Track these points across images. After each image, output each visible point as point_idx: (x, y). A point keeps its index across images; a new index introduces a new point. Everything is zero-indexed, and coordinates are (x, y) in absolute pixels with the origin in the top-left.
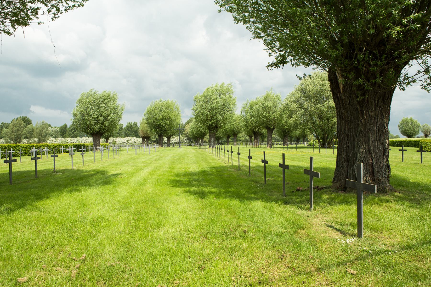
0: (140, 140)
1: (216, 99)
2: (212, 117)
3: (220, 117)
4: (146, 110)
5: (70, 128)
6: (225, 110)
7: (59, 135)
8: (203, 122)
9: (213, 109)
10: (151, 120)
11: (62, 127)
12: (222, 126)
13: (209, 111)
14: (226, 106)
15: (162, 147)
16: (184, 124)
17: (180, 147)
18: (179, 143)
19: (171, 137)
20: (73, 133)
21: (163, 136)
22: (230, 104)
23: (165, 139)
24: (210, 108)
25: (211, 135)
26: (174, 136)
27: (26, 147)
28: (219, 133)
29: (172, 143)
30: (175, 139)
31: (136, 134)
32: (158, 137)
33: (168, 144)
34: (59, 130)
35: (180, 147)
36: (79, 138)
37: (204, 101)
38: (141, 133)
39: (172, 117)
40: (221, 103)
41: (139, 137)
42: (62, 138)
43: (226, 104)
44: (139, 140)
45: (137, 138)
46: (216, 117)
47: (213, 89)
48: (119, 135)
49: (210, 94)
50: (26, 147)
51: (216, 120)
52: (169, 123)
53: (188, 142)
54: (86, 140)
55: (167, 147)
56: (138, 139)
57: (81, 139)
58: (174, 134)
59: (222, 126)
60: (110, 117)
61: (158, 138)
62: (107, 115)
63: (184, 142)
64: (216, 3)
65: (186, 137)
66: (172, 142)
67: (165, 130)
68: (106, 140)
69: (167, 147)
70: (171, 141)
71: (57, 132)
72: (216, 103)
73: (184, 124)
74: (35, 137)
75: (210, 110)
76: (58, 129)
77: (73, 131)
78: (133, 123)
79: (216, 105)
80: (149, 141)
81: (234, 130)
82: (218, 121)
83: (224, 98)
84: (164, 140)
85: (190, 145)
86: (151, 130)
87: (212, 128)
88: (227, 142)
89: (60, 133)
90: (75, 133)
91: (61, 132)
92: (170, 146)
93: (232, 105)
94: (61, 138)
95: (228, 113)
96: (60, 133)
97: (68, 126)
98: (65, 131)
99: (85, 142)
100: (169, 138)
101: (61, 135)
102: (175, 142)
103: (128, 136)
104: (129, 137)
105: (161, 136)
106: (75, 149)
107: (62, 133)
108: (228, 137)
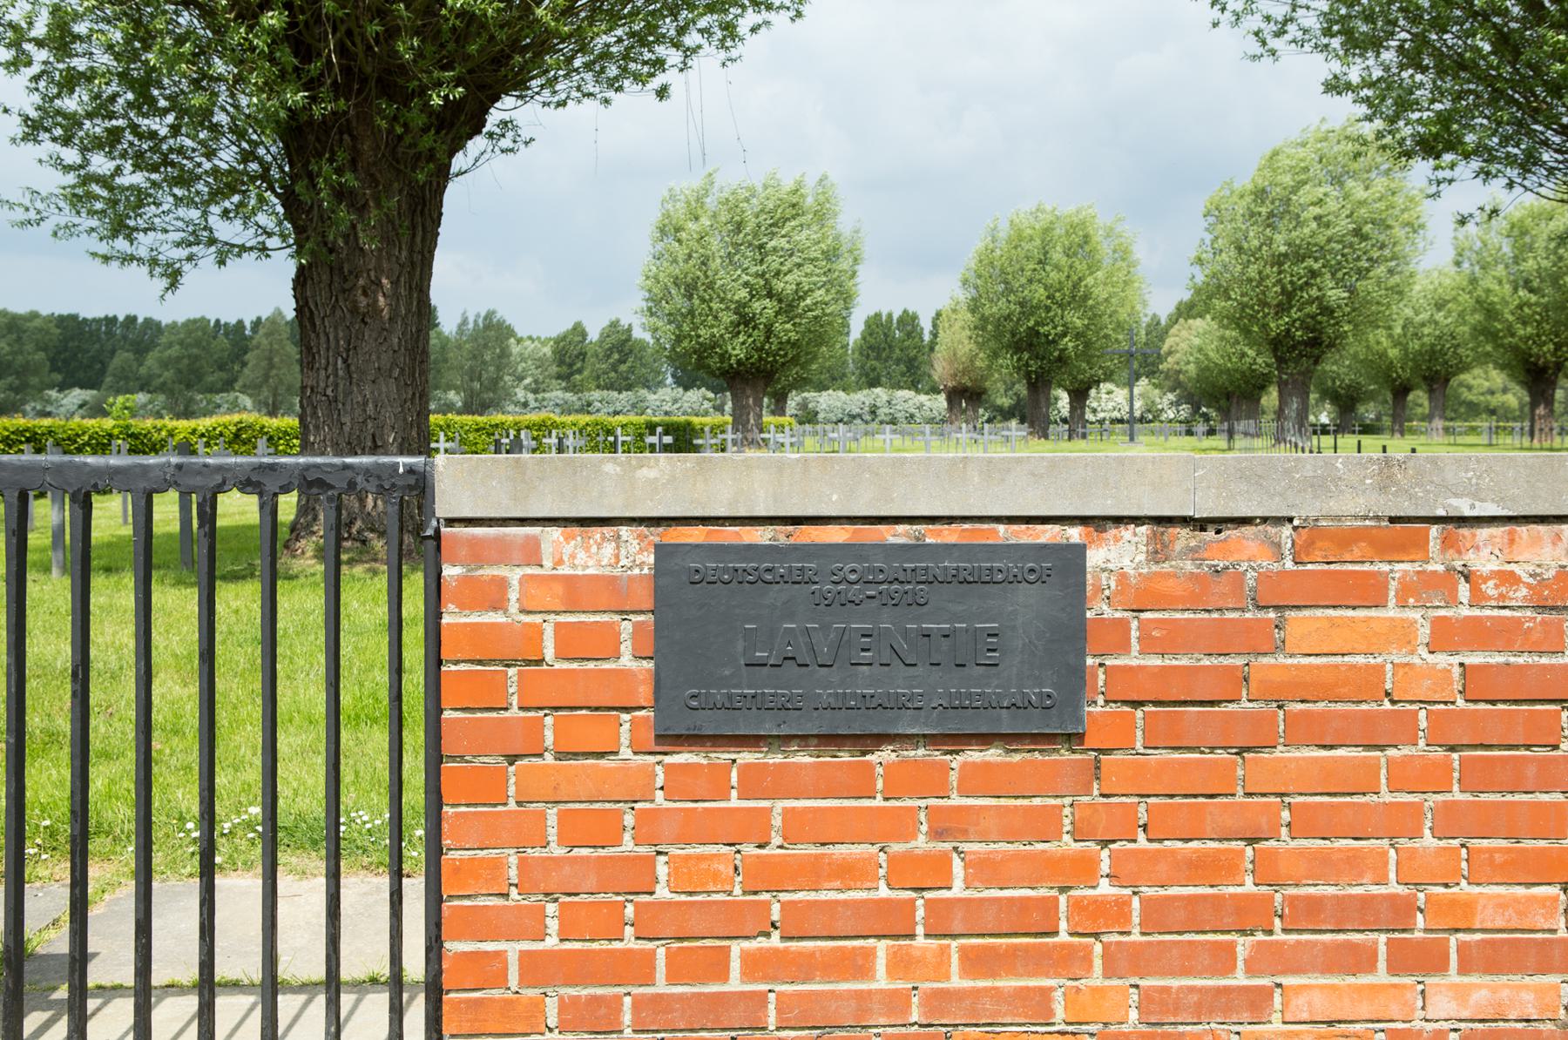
0: (941, 401)
1: (1319, 202)
2: (1289, 295)
3: (1335, 295)
4: (969, 260)
5: (601, 342)
6: (1358, 260)
7: (551, 377)
8: (1242, 320)
9: (1298, 254)
10: (999, 308)
11: (564, 338)
12: (1344, 335)
13: (1279, 260)
14: (1365, 238)
15: (1046, 437)
16: (1163, 322)
17: (1132, 439)
18: (1131, 424)
19: (1093, 392)
20: (614, 368)
21: (1048, 385)
22: (1389, 227)
23: (1063, 401)
24: (1283, 249)
25: (1286, 383)
26: (1105, 387)
27: (477, 430)
28: (1337, 367)
29: (1101, 422)
30: (1109, 399)
31: (913, 373)
32: (1022, 389)
33: (1076, 425)
34: (549, 354)
35: (1132, 439)
36: (643, 392)
37: (1252, 215)
38: (941, 369)
39: (1101, 293)
40: (1343, 226)
41: (934, 390)
42: (566, 389)
43: (1367, 228)
44: (928, 404)
45: (918, 391)
46: (1314, 292)
47: (1302, 152)
48: (833, 379)
49: (1287, 180)
50: (477, 430)
51: (1314, 308)
52: (1078, 323)
53: (1184, 415)
54: (675, 401)
55: (1070, 438)
56: (923, 398)
57: (651, 397)
58: (1109, 377)
59: (1344, 335)
60: (808, 301)
61: (1024, 392)
62: (796, 292)
63: (1164, 417)
64: (1213, 5)
65: (1172, 390)
66: (1101, 415)
67: (1060, 359)
68: (778, 401)
69: (1070, 438)
70: (1094, 411)
71: (540, 363)
72: (1314, 225)
73: (1163, 322)
74: (449, 387)
75: (1286, 255)
76: (547, 350)
77: (616, 356)
78: (895, 317)
79: (1313, 235)
80: (981, 411)
81: (1433, 353)
82: (1327, 311)
83: (1360, 194)
84: (1060, 404)
85: (1189, 433)
86: (995, 355)
87: (1294, 347)
88: (1400, 421)
89: (554, 369)
90: (623, 368)
91: (561, 363)
92: (1084, 436)
93: (1399, 232)
94: (559, 393)
95: (1380, 270)
96: (554, 369)
97: (594, 335)
98: (577, 357)
99: (666, 413)
100: (1079, 396)
101: (559, 377)
102: (1116, 414)
103: (874, 383)
104: (878, 390)
105: (1039, 384)
106: (401, 470)
107: (565, 369)
108: (1401, 392)
